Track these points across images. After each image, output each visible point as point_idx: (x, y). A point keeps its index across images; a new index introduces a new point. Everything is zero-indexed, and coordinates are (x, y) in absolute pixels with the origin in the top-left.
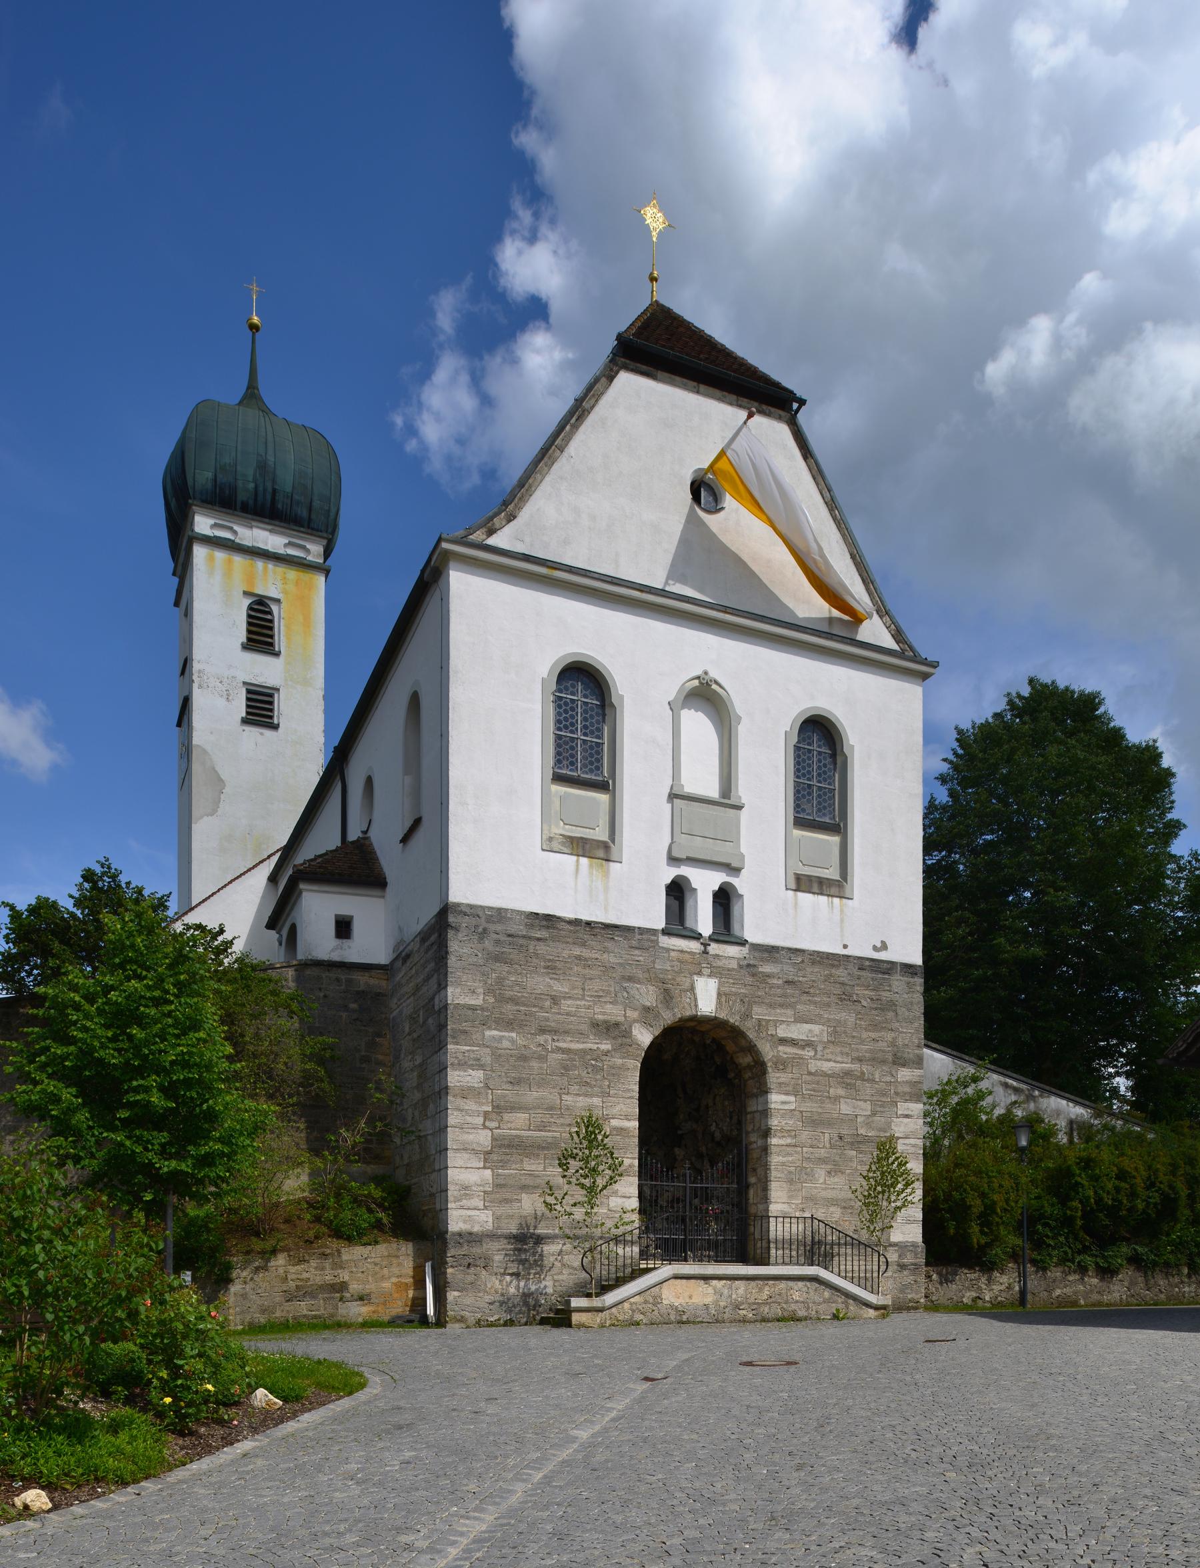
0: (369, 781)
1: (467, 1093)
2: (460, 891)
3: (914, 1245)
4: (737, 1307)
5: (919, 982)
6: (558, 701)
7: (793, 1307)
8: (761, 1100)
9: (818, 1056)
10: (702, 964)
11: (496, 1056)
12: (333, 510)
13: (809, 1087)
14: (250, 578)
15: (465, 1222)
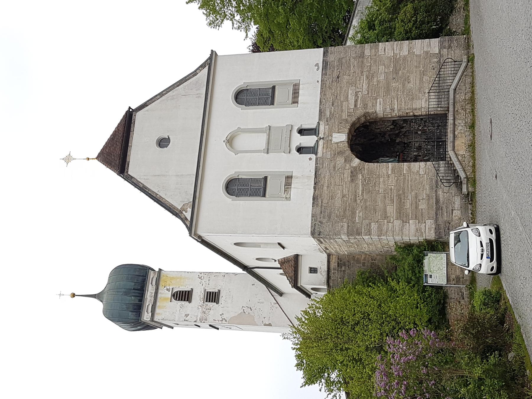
3: (440, 42)
10: (327, 139)
12: (139, 267)
15: (431, 231)
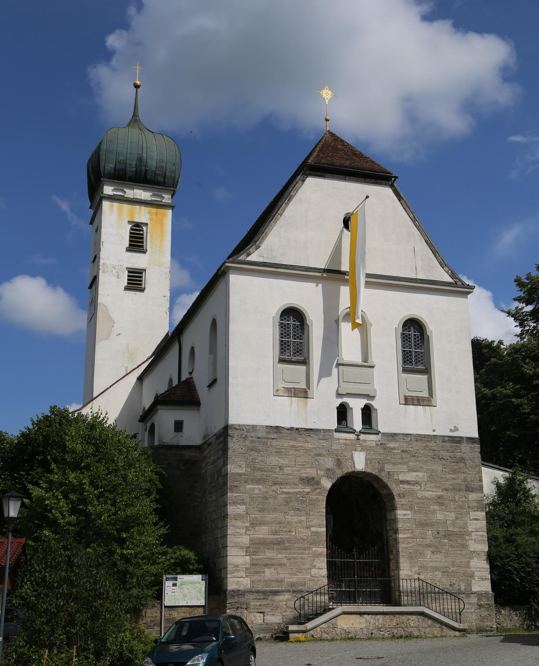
0: (192, 350)
1: (238, 517)
2: (233, 420)
3: (487, 593)
4: (379, 629)
5: (477, 447)
6: (282, 325)
7: (411, 630)
8: (393, 513)
9: (423, 489)
10: (357, 445)
11: (252, 498)
13: (419, 506)
14: (132, 214)
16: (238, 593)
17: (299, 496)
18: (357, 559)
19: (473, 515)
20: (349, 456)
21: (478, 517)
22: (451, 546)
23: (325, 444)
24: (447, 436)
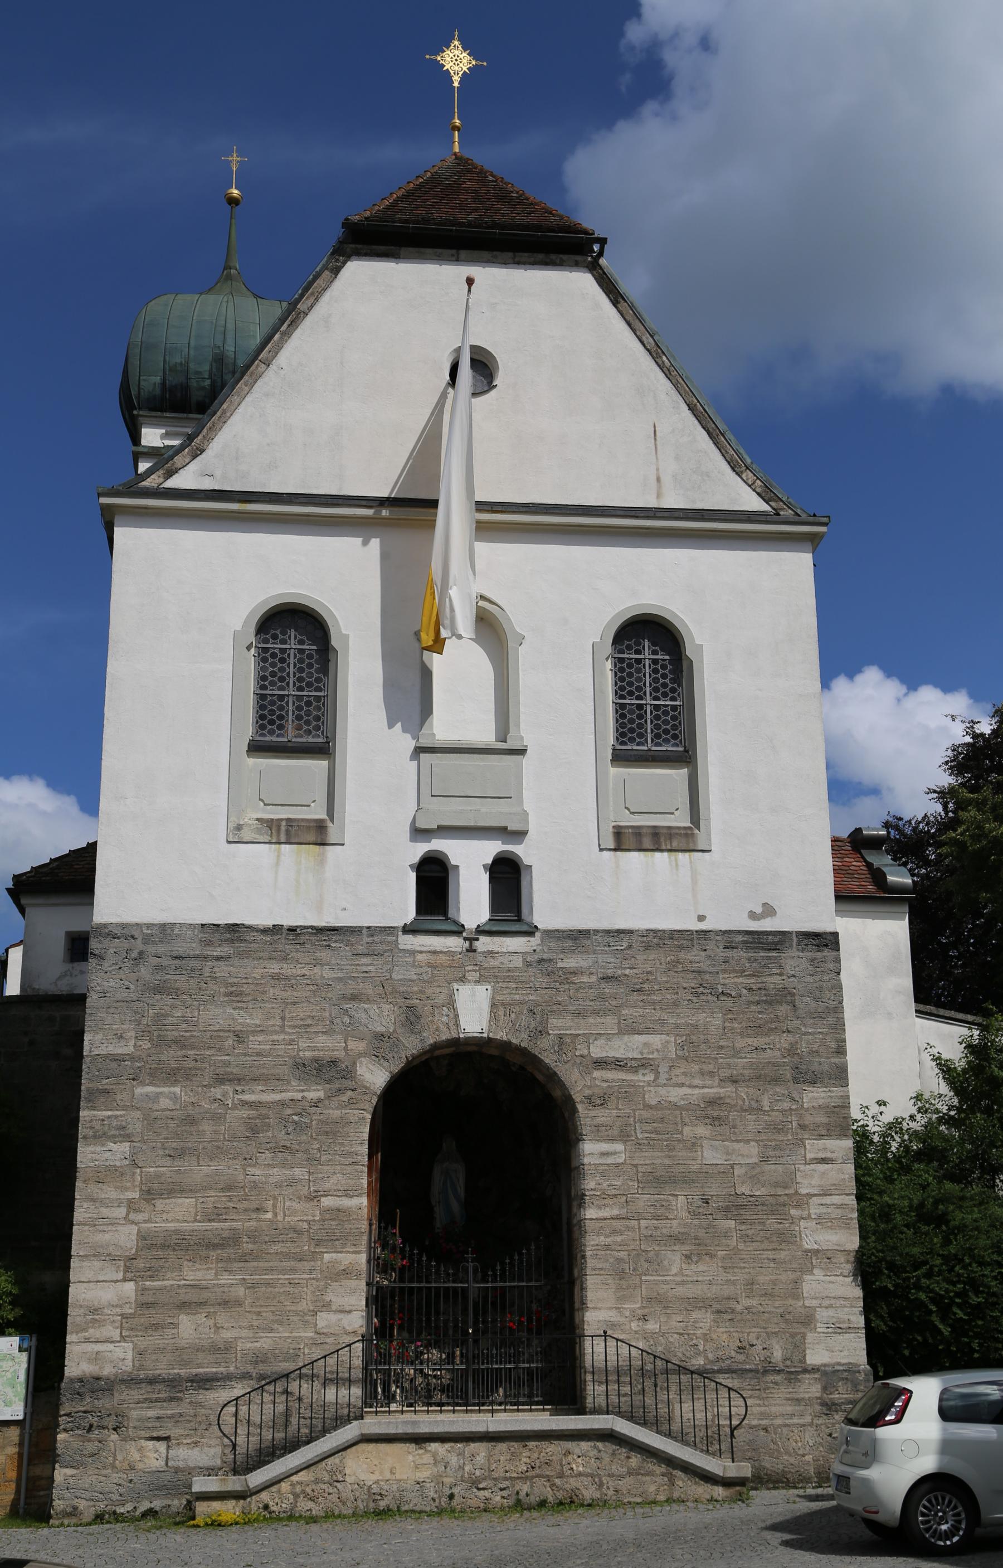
1: (106, 1174)
3: (851, 1370)
4: (475, 1483)
6: (264, 656)
7: (573, 1483)
9: (662, 1080)
10: (469, 965)
11: (150, 1121)
13: (649, 1127)
16: (96, 1386)
17: (289, 1111)
18: (476, 1281)
19: (814, 1148)
20: (442, 997)
21: (829, 1155)
22: (746, 1238)
23: (371, 968)
24: (739, 932)
